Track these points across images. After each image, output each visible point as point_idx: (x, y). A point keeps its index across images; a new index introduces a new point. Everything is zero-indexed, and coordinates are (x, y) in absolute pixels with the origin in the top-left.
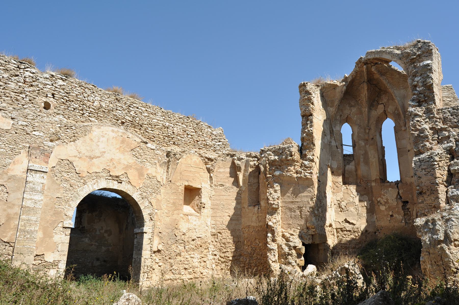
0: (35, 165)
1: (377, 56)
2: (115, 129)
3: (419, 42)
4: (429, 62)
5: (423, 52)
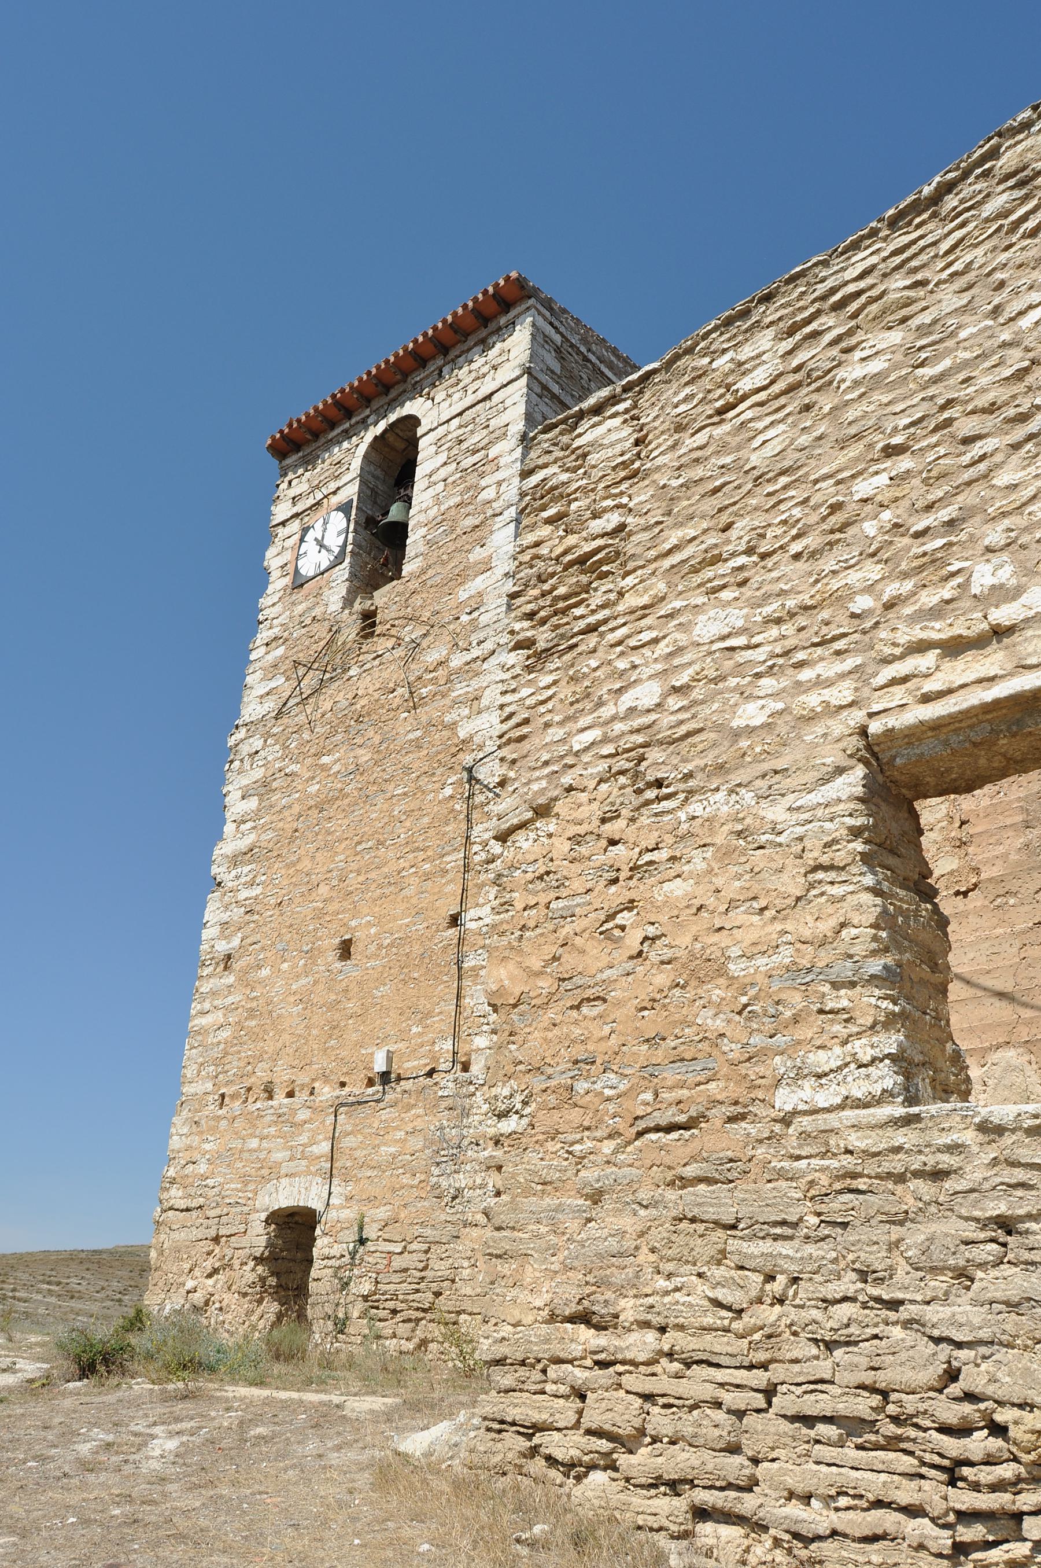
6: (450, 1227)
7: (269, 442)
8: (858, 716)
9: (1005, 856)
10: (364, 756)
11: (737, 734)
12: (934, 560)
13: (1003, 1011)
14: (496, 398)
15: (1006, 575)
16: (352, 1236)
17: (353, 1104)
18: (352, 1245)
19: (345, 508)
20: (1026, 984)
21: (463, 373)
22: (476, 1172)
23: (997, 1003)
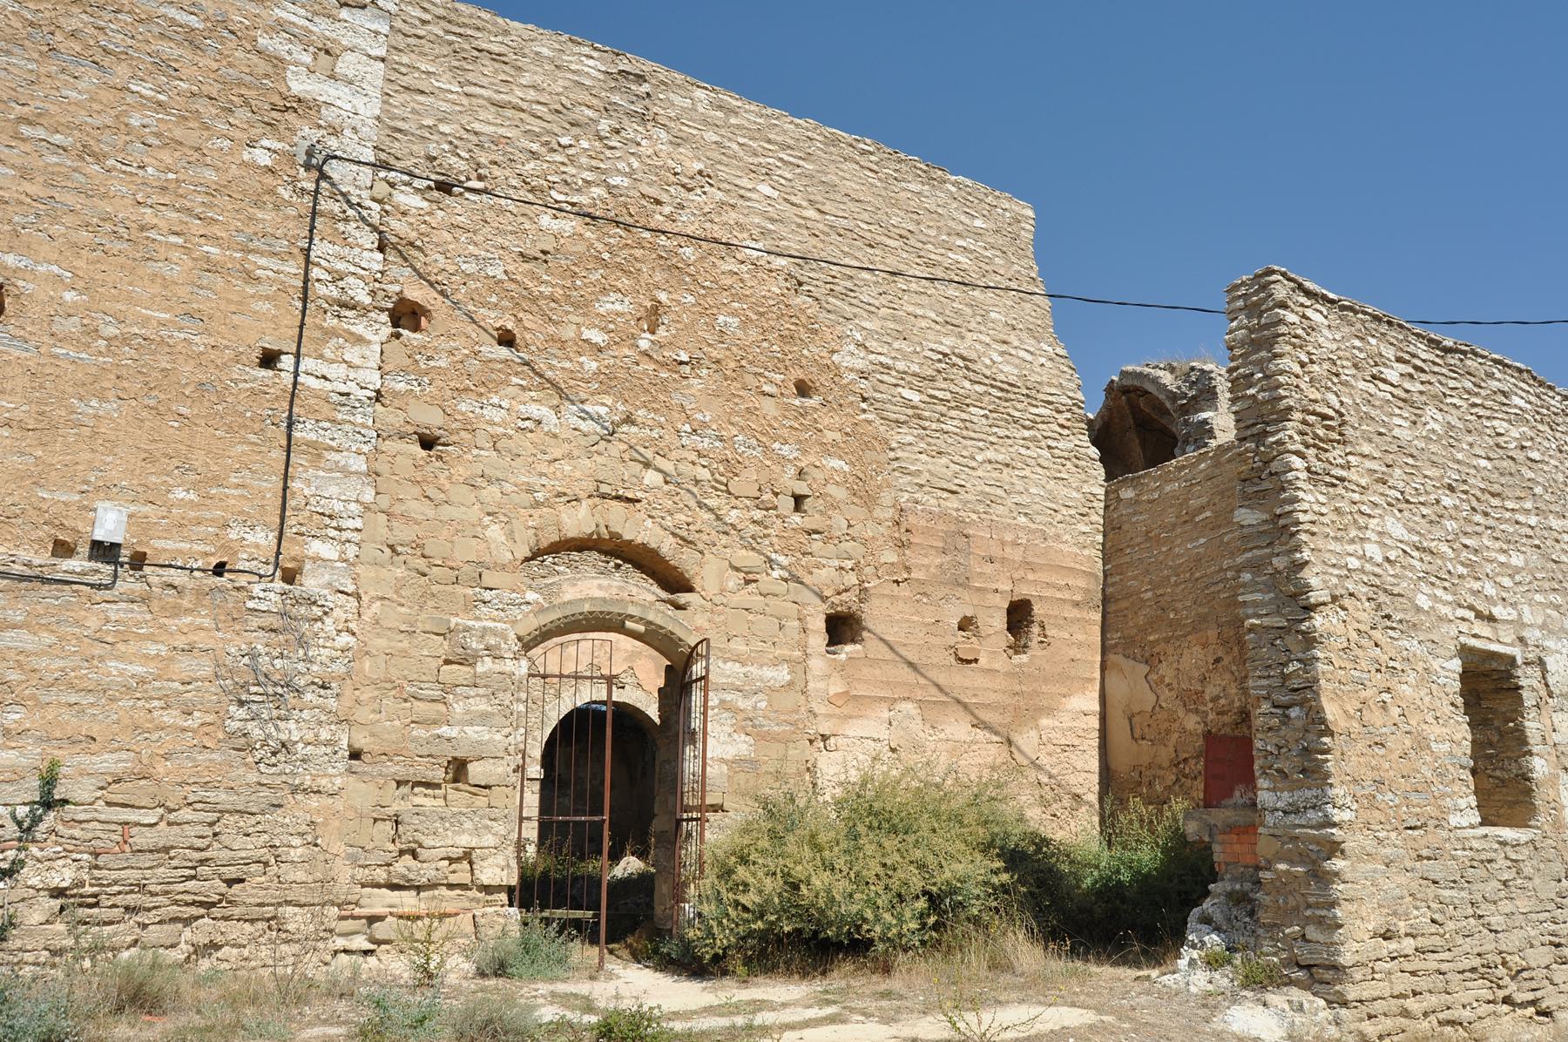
0: (441, 33)
1: (1137, 383)
2: (604, 582)
3: (1193, 369)
4: (1204, 415)
5: (1201, 392)
6: (265, 792)
9: (927, 567)
13: (906, 674)
16: (31, 789)
17: (22, 578)
18: (22, 811)
20: (924, 660)
22: (320, 723)
23: (907, 670)
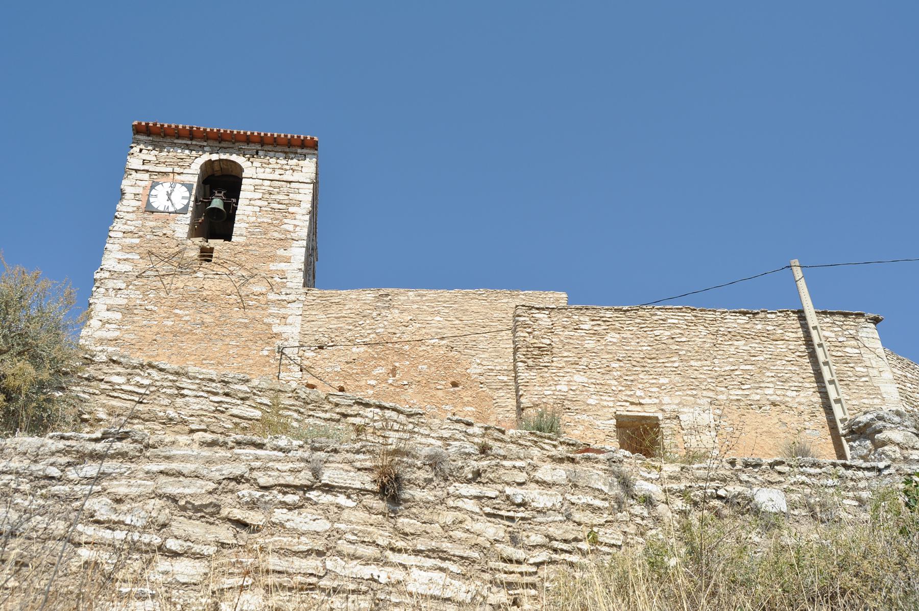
7: (136, 123)
8: (614, 410)
10: (208, 319)
11: (588, 405)
12: (629, 386)
14: (293, 185)
15: (642, 394)
19: (189, 187)
21: (273, 161)
